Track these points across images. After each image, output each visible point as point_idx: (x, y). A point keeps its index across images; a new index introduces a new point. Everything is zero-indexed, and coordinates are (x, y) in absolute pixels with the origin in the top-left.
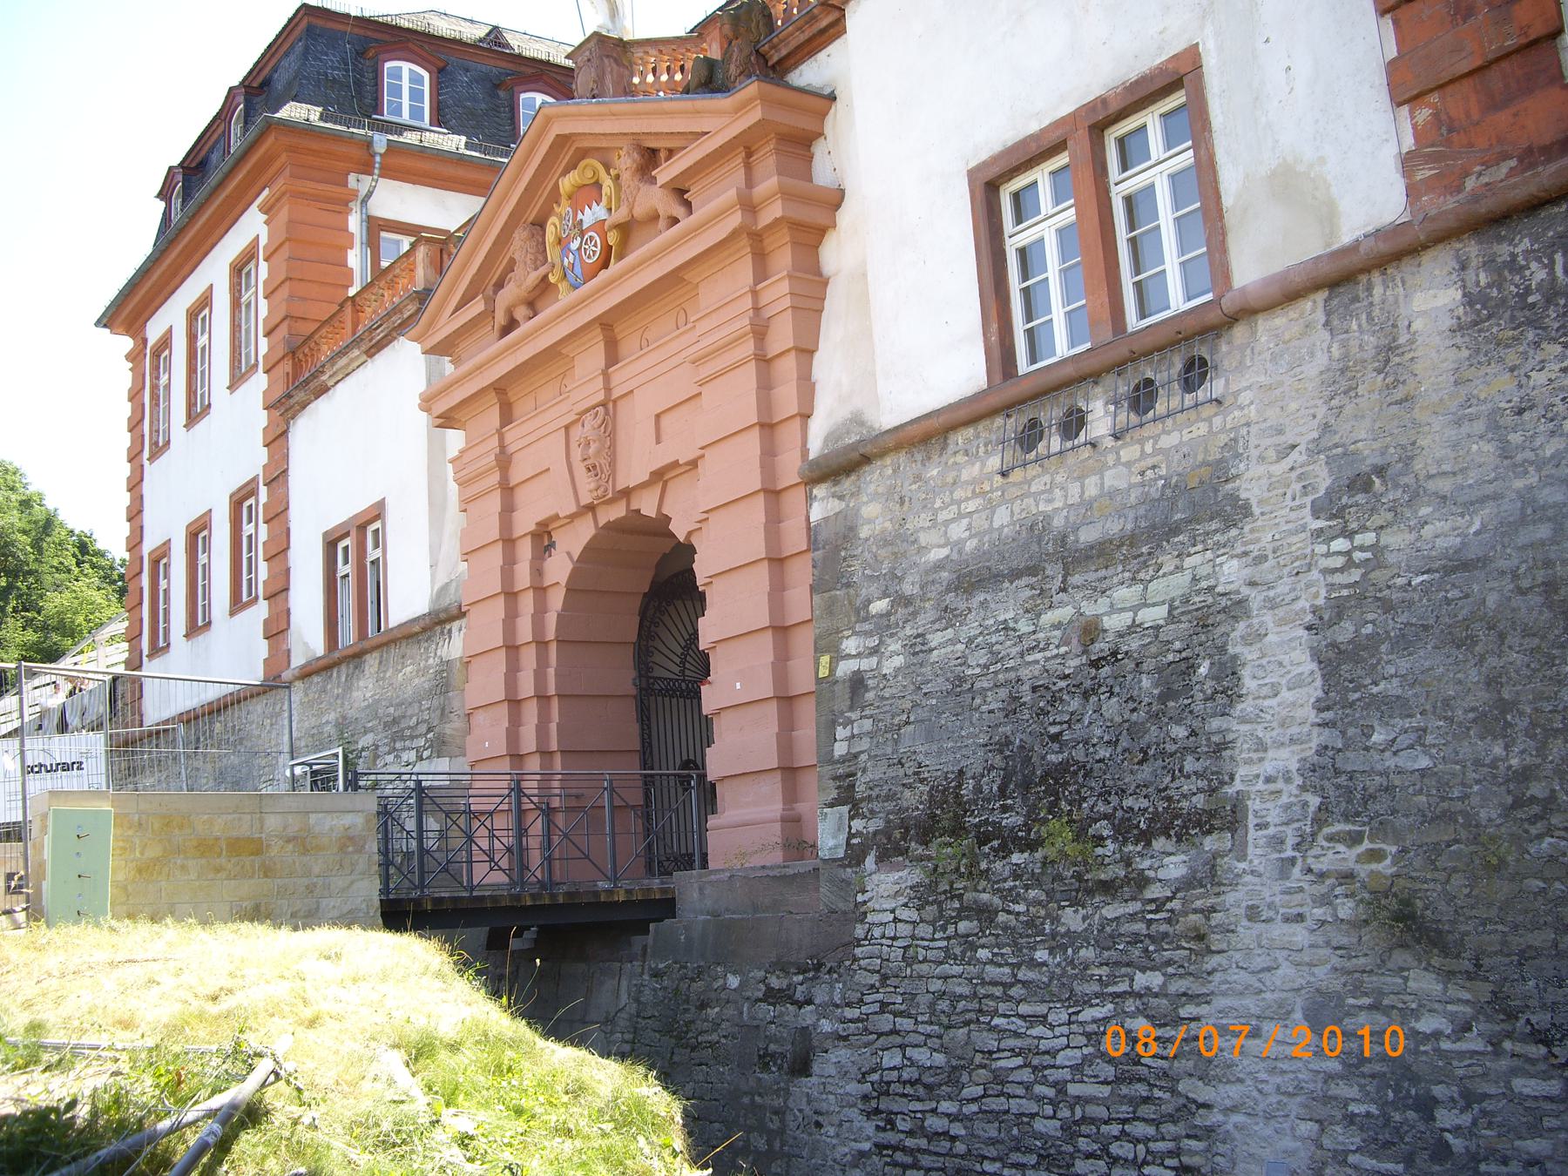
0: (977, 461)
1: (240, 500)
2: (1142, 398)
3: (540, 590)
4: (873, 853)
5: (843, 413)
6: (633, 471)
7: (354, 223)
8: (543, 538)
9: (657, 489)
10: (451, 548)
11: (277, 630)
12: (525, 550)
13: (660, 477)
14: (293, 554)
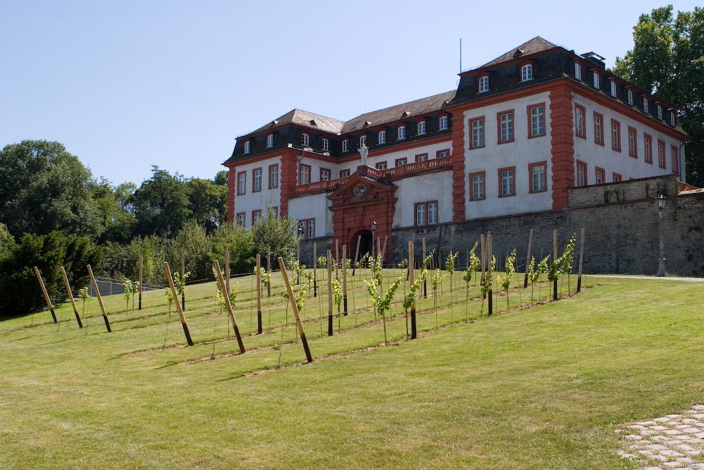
2: (429, 231)
4: (13, 379)
5: (396, 224)
8: (349, 230)
12: (346, 231)
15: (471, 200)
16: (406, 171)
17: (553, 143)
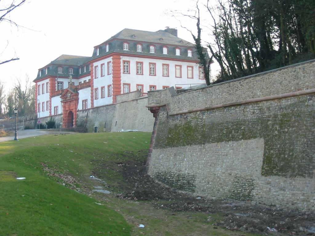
0: (81, 112)
1: (47, 102)
3: (67, 114)
6: (71, 109)
7: (56, 82)
9: (197, 38)
10: (62, 110)
11: (50, 112)
13: (72, 109)
14: (52, 108)
15: (95, 99)
16: (212, 51)
17: (113, 77)
